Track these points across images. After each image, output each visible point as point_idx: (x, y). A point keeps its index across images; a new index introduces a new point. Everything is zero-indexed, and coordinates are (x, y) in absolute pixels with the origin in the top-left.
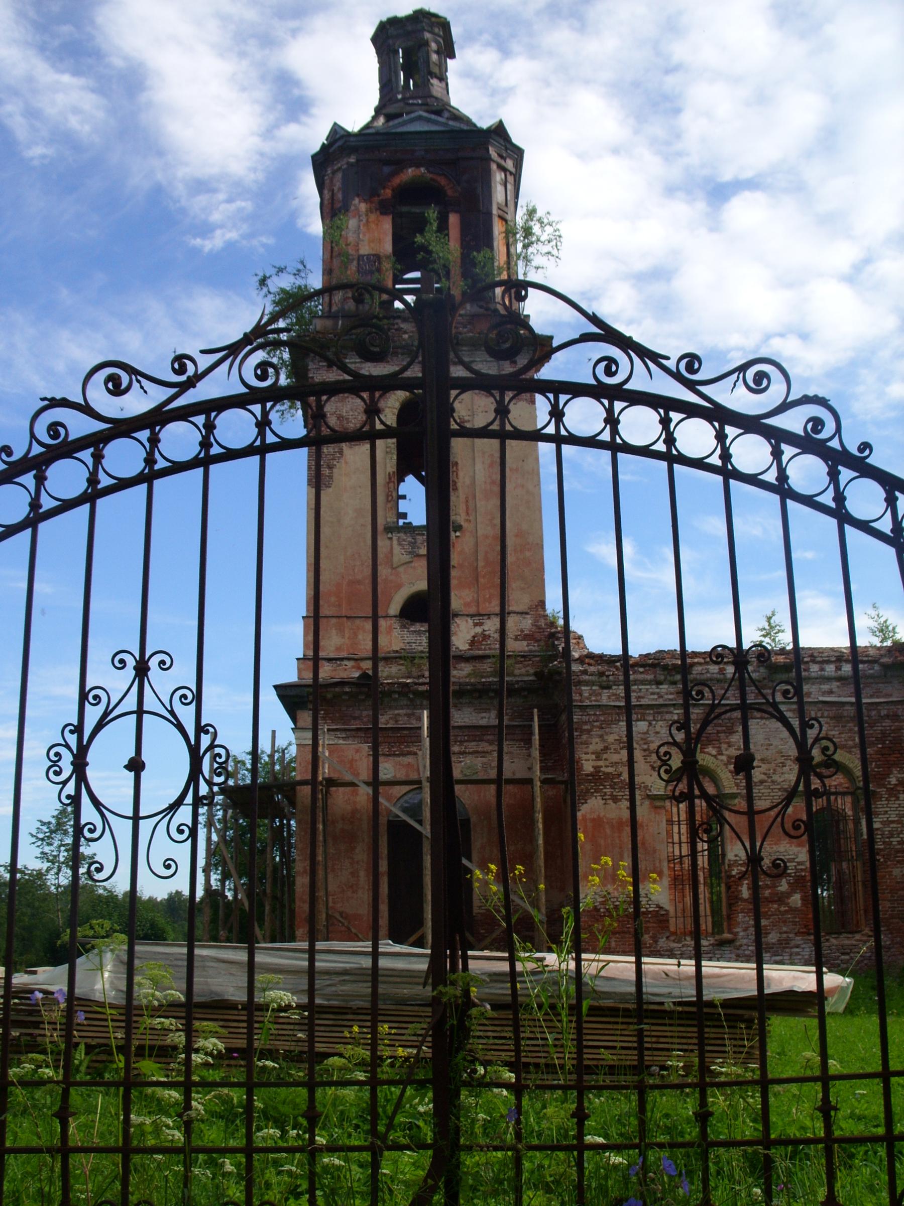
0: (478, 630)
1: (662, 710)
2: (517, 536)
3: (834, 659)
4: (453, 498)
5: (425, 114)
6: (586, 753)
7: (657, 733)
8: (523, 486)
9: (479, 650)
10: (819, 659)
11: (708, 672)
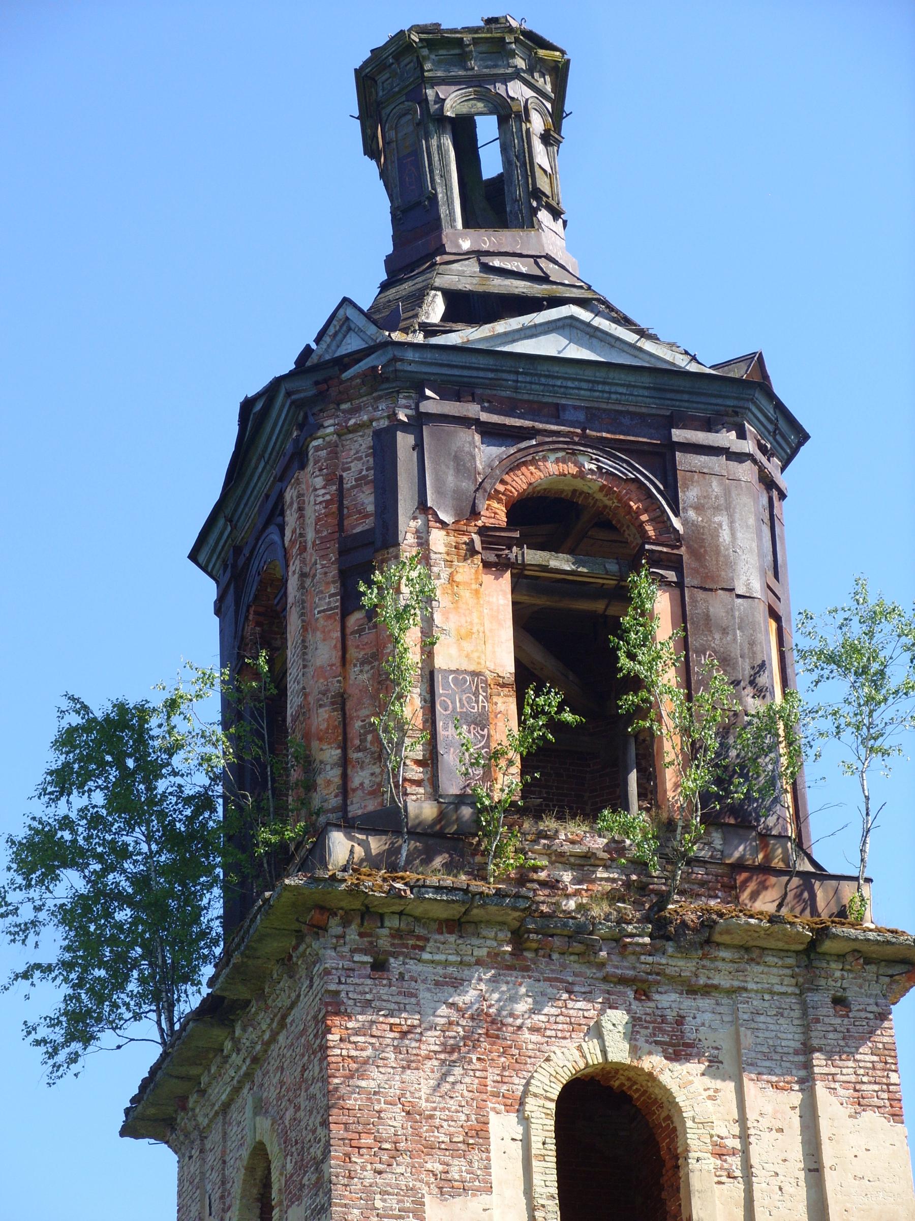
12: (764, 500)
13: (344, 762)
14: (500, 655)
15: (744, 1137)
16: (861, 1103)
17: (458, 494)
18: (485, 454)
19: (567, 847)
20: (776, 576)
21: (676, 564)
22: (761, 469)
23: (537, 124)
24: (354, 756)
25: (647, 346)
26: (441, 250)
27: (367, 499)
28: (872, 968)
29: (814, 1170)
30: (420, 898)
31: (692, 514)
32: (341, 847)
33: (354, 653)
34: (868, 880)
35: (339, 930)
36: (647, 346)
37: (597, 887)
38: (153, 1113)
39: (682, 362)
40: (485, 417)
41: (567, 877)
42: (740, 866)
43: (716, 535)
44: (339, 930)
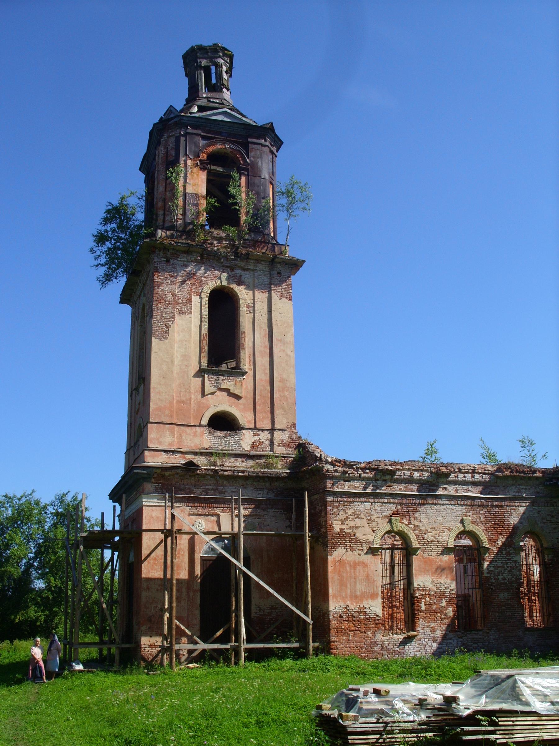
0: (256, 438)
1: (503, 504)
2: (280, 381)
3: (471, 471)
4: (242, 354)
5: (229, 111)
6: (336, 520)
7: (376, 510)
8: (284, 351)
9: (256, 451)
10: (463, 471)
11: (404, 475)
12: (271, 157)
13: (164, 215)
14: (203, 190)
15: (254, 303)
16: (282, 296)
17: (195, 152)
18: (202, 143)
19: (216, 235)
20: (273, 175)
21: (247, 170)
22: (270, 149)
23: (224, 68)
24: (167, 213)
25: (244, 119)
26: (198, 97)
27: (173, 153)
28: (287, 266)
29: (270, 311)
30: (177, 245)
31: (252, 158)
32: (160, 233)
33: (168, 189)
34: (288, 246)
35: (158, 252)
36: (244, 119)
37: (223, 245)
38: (125, 298)
39: (252, 123)
40: (202, 134)
41: (215, 242)
42: (258, 241)
43: (257, 163)
44: (158, 252)
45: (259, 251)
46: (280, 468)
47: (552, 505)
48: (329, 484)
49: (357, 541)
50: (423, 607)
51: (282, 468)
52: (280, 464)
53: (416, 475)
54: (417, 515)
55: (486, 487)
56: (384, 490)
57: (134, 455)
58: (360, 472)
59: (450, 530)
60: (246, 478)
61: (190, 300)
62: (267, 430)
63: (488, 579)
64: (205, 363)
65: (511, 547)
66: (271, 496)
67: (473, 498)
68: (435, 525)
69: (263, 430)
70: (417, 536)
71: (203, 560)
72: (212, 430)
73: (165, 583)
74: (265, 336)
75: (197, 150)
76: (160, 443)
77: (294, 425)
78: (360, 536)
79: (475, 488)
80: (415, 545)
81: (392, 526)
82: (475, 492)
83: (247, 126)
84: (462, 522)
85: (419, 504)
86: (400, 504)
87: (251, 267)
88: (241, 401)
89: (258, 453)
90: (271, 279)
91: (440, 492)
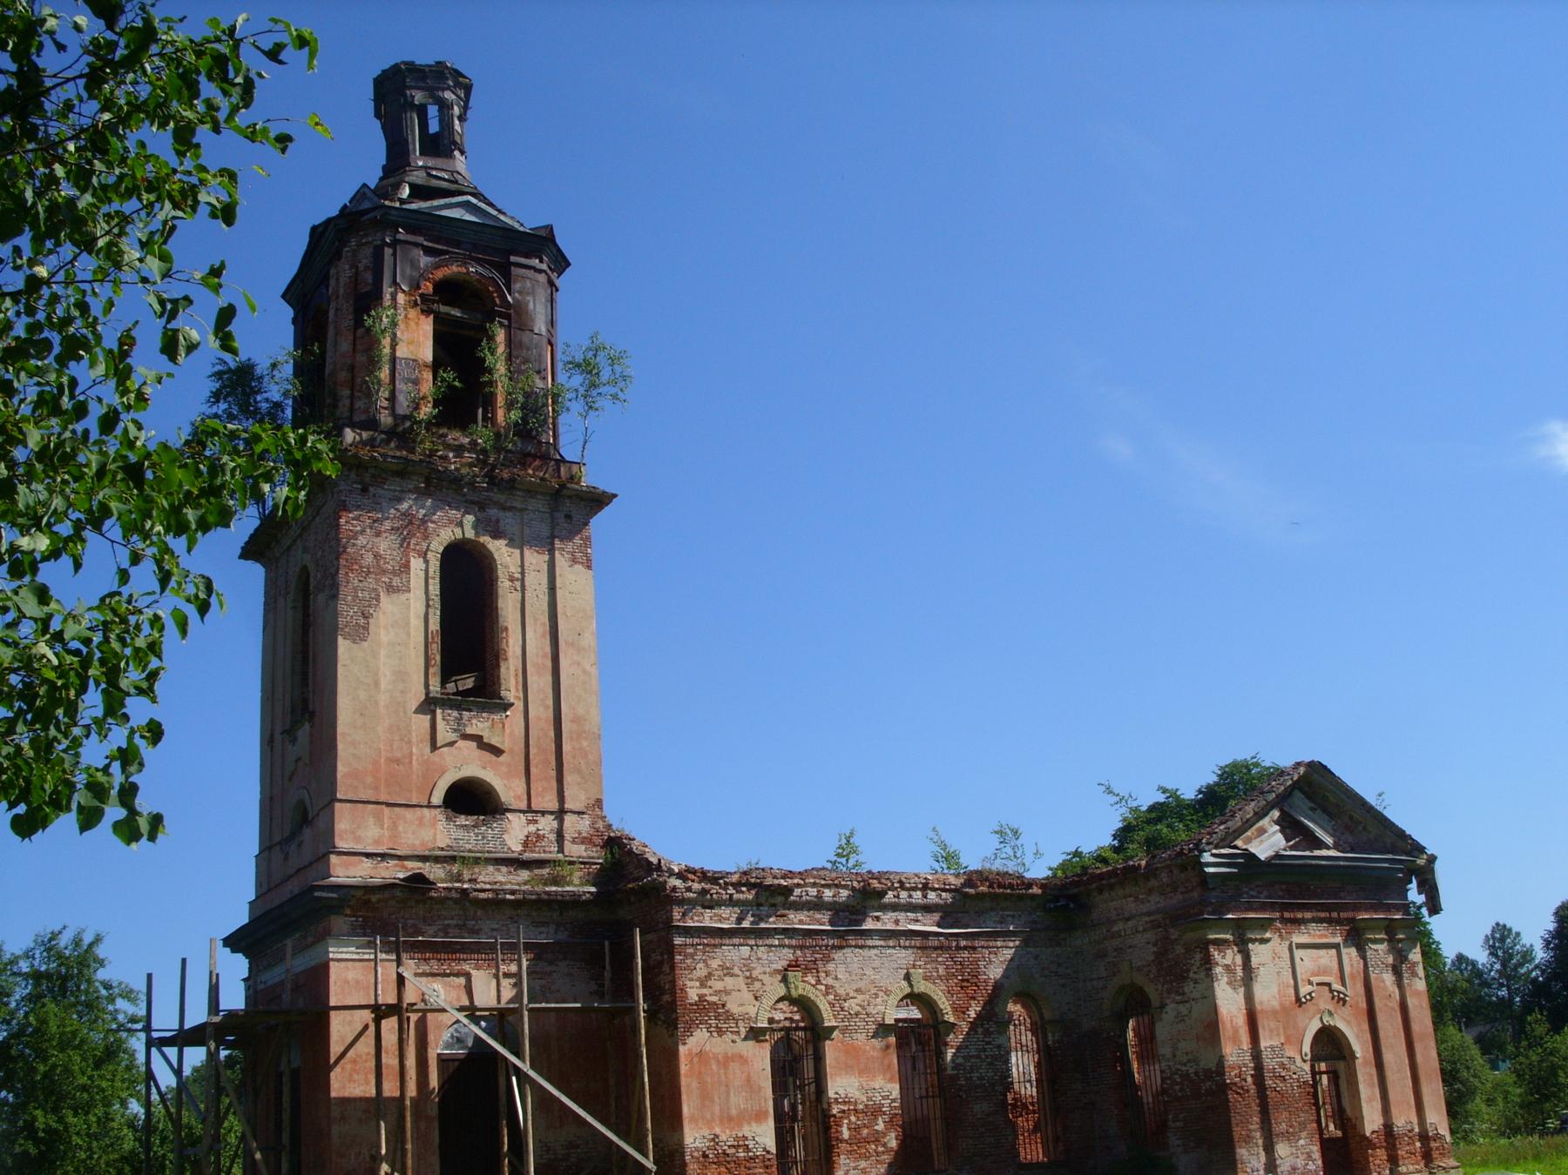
0: (532, 828)
1: (976, 944)
13: (352, 397)
14: (427, 354)
15: (523, 573)
16: (574, 561)
18: (425, 261)
21: (508, 317)
23: (456, 111)
29: (552, 589)
36: (502, 217)
39: (517, 226)
42: (529, 454)
45: (531, 474)
46: (579, 885)
47: (1059, 944)
48: (676, 915)
49: (729, 1016)
50: (846, 1134)
51: (582, 885)
52: (577, 877)
53: (828, 894)
54: (831, 967)
55: (948, 914)
56: (772, 923)
57: (286, 858)
58: (731, 891)
59: (887, 992)
60: (517, 904)
61: (407, 566)
62: (552, 813)
63: (954, 1078)
64: (435, 687)
65: (991, 1021)
66: (562, 936)
67: (925, 935)
68: (861, 984)
69: (543, 813)
70: (832, 1005)
71: (442, 1060)
72: (451, 814)
73: (376, 1106)
74: (543, 636)
75: (415, 274)
76: (357, 839)
77: (599, 803)
78: (733, 1007)
79: (929, 916)
80: (829, 1022)
81: (788, 988)
82: (928, 925)
83: (509, 232)
84: (907, 977)
85: (833, 947)
86: (801, 947)
87: (517, 504)
88: (502, 758)
89: (536, 856)
90: (553, 528)
91: (869, 925)
